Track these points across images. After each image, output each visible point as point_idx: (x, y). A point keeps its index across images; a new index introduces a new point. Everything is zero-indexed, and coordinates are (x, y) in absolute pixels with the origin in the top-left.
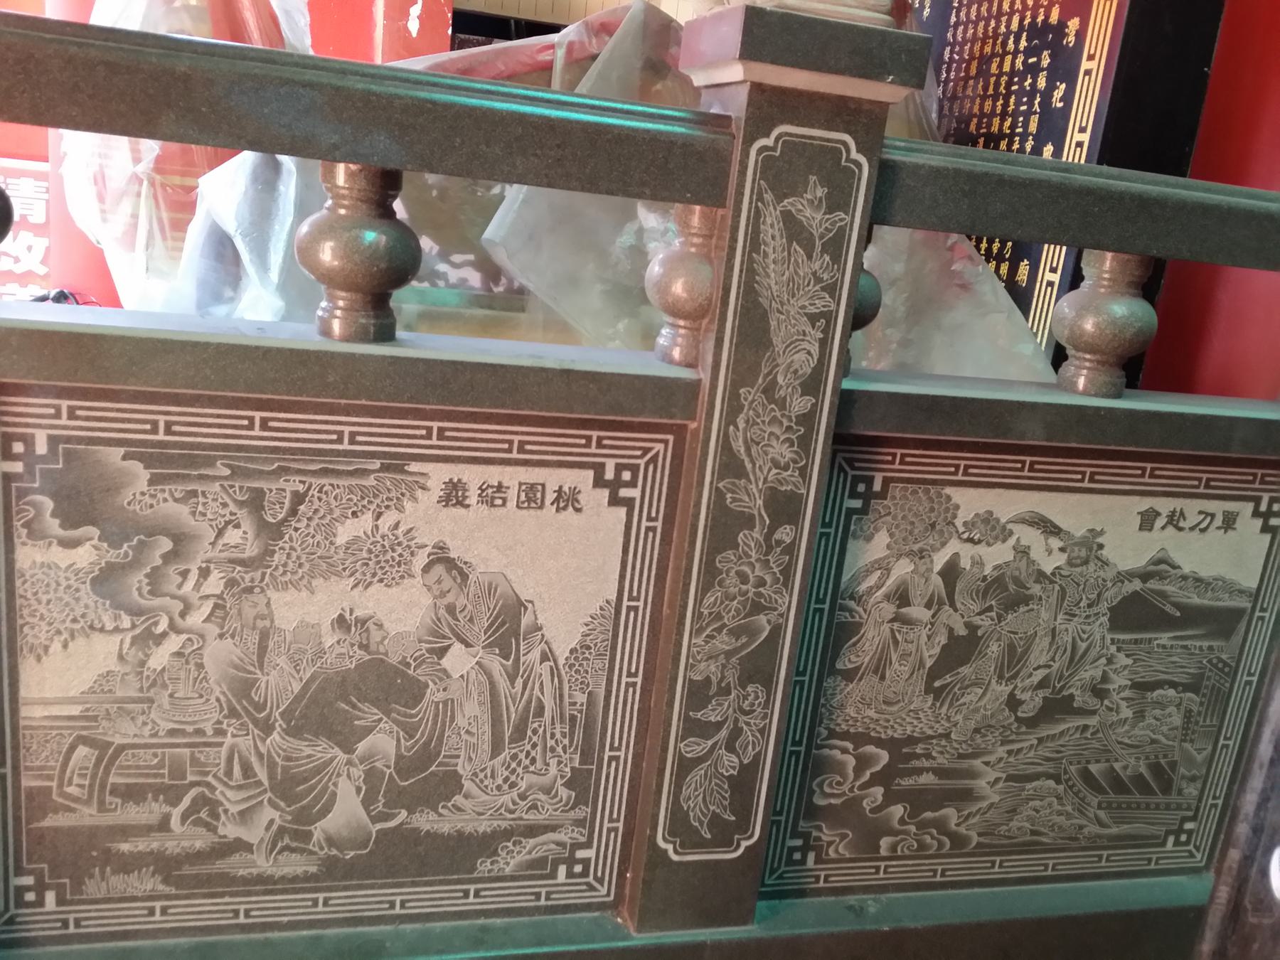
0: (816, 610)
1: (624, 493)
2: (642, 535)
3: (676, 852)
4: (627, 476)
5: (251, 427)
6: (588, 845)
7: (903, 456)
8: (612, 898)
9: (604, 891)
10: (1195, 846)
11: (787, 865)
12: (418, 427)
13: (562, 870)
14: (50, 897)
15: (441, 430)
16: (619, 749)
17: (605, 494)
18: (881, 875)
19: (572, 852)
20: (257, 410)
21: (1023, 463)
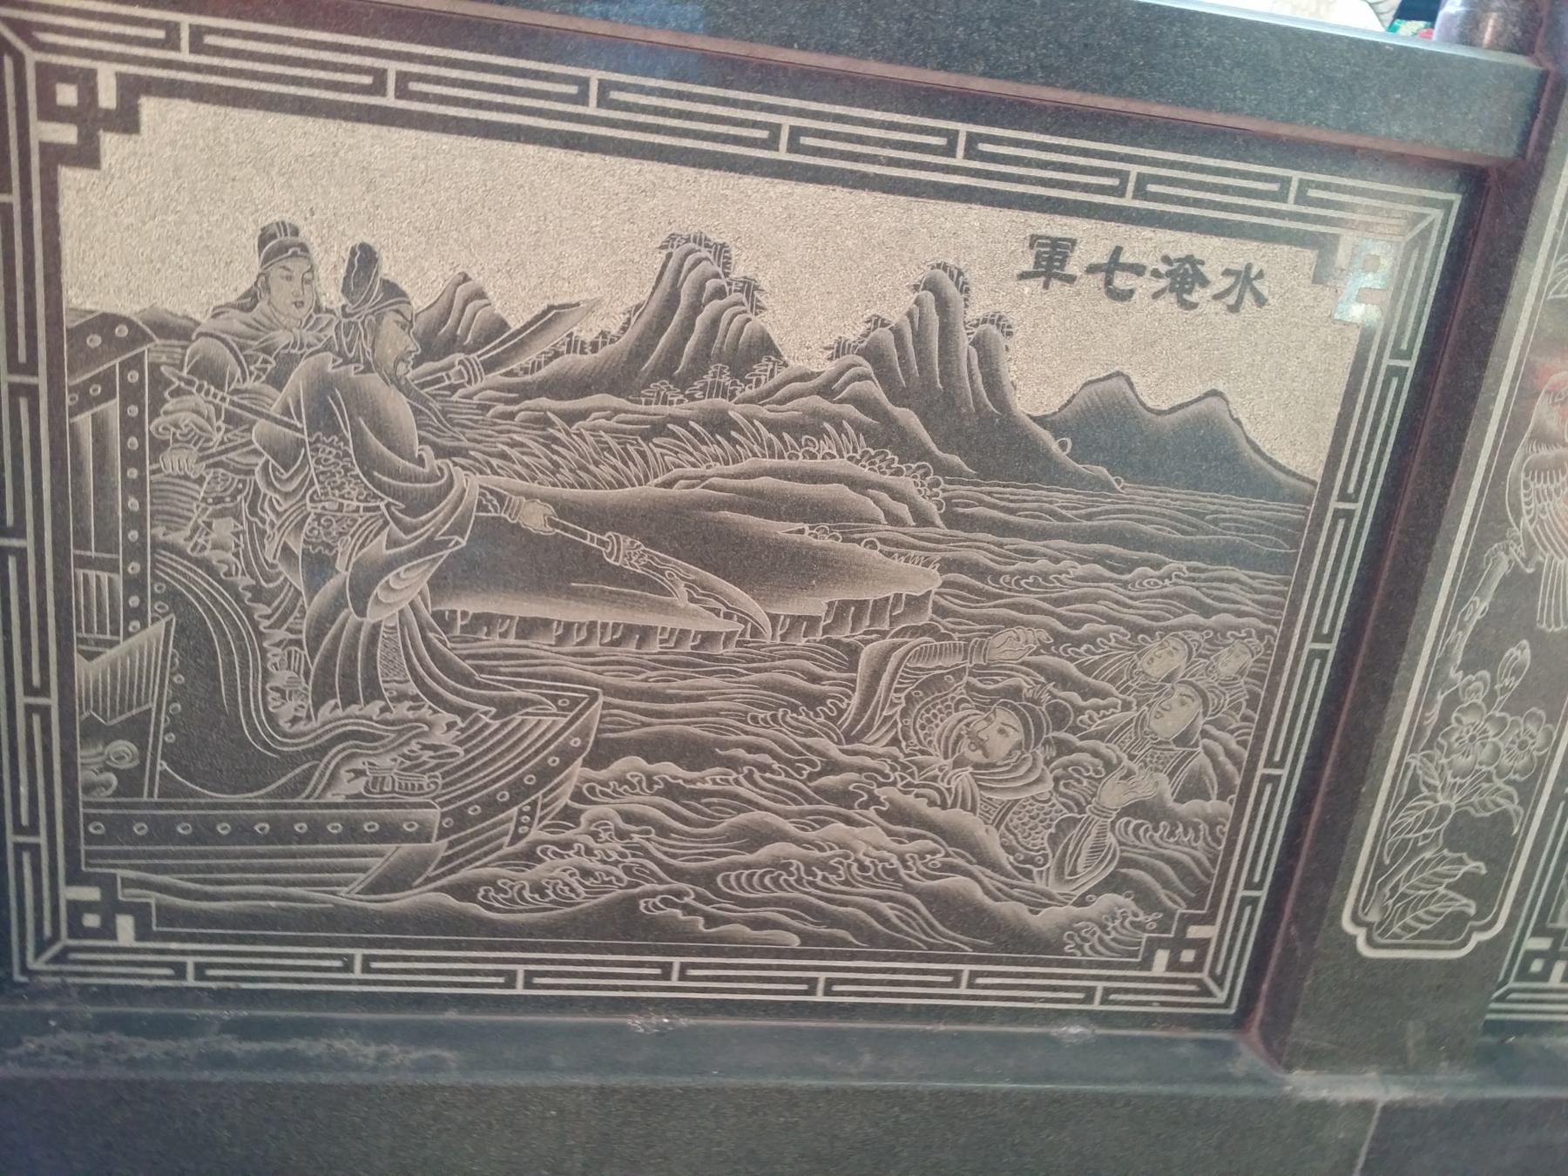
0: (1338, 514)
1: (107, 98)
2: (1381, 379)
3: (1370, 941)
4: (67, 95)
5: (1142, 180)
6: (1208, 920)
7: (1304, 184)
8: (1232, 1011)
9: (1221, 996)
10: (1212, 975)
11: (1518, 979)
12: (150, 23)
13: (1162, 957)
14: (125, 926)
15: (972, 139)
16: (1281, 765)
17: (111, 144)
18: (674, 981)
19: (1182, 930)
20: (963, 121)
21: (1285, 182)
